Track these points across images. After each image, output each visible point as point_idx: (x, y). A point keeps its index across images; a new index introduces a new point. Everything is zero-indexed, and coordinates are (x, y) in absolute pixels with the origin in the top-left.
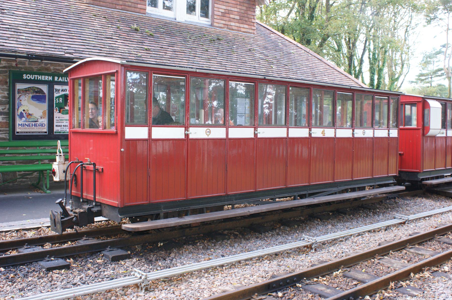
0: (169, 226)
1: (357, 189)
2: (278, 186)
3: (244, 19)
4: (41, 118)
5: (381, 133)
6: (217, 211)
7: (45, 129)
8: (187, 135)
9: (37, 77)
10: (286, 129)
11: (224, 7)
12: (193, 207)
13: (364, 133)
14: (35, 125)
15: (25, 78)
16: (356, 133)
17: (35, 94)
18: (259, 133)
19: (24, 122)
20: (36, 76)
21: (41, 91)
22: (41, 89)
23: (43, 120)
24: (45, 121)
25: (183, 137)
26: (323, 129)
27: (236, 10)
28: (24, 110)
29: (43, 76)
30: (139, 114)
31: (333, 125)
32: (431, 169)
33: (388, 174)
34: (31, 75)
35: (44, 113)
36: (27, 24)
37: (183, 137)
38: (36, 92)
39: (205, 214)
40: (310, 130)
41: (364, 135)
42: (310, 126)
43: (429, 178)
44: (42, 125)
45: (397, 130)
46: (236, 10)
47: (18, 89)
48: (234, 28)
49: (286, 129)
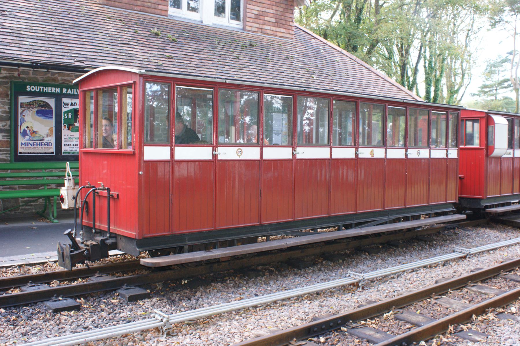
0: (195, 261)
1: (410, 218)
2: (320, 215)
3: (281, 21)
4: (47, 136)
5: (439, 154)
7: (52, 149)
8: (215, 156)
9: (43, 89)
10: (329, 148)
11: (258, 9)
12: (222, 238)
13: (419, 153)
14: (41, 144)
15: (28, 90)
16: (410, 154)
17: (40, 108)
18: (298, 153)
19: (28, 140)
20: (42, 88)
21: (47, 105)
22: (47, 103)
23: (49, 138)
24: (52, 140)
25: (210, 158)
26: (371, 149)
27: (271, 11)
28: (28, 127)
29: (49, 88)
30: (160, 132)
31: (383, 144)
32: (496, 195)
33: (446, 201)
34: (36, 87)
35: (51, 130)
36: (31, 28)
37: (210, 158)
38: (42, 106)
39: (236, 247)
40: (357, 150)
41: (419, 155)
42: (356, 146)
43: (493, 205)
44: (48, 144)
45: (457, 150)
46: (271, 11)
47: (21, 103)
48: (269, 32)
49: (329, 148)
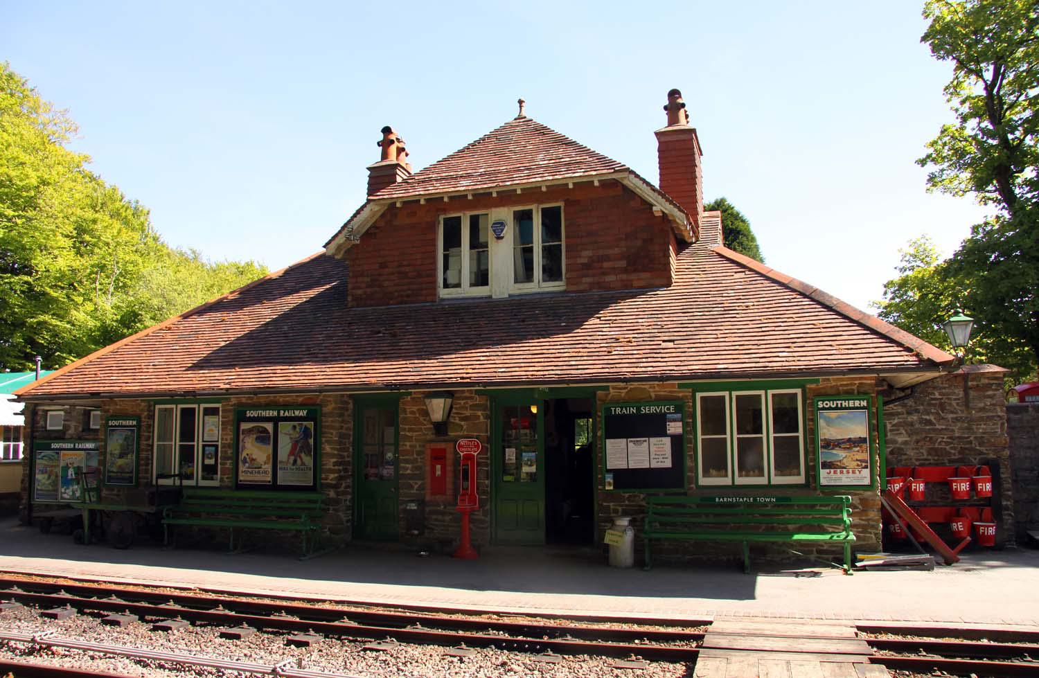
4: (265, 463)
6: (956, 630)
7: (269, 478)
9: (841, 404)
14: (259, 472)
15: (248, 415)
17: (259, 434)
19: (249, 468)
20: (839, 402)
21: (265, 431)
22: (265, 428)
23: (266, 466)
24: (269, 467)
28: (247, 455)
29: (268, 411)
30: (415, 456)
34: (831, 402)
35: (268, 457)
36: (759, 347)
38: (261, 432)
44: (265, 472)
47: (243, 430)
